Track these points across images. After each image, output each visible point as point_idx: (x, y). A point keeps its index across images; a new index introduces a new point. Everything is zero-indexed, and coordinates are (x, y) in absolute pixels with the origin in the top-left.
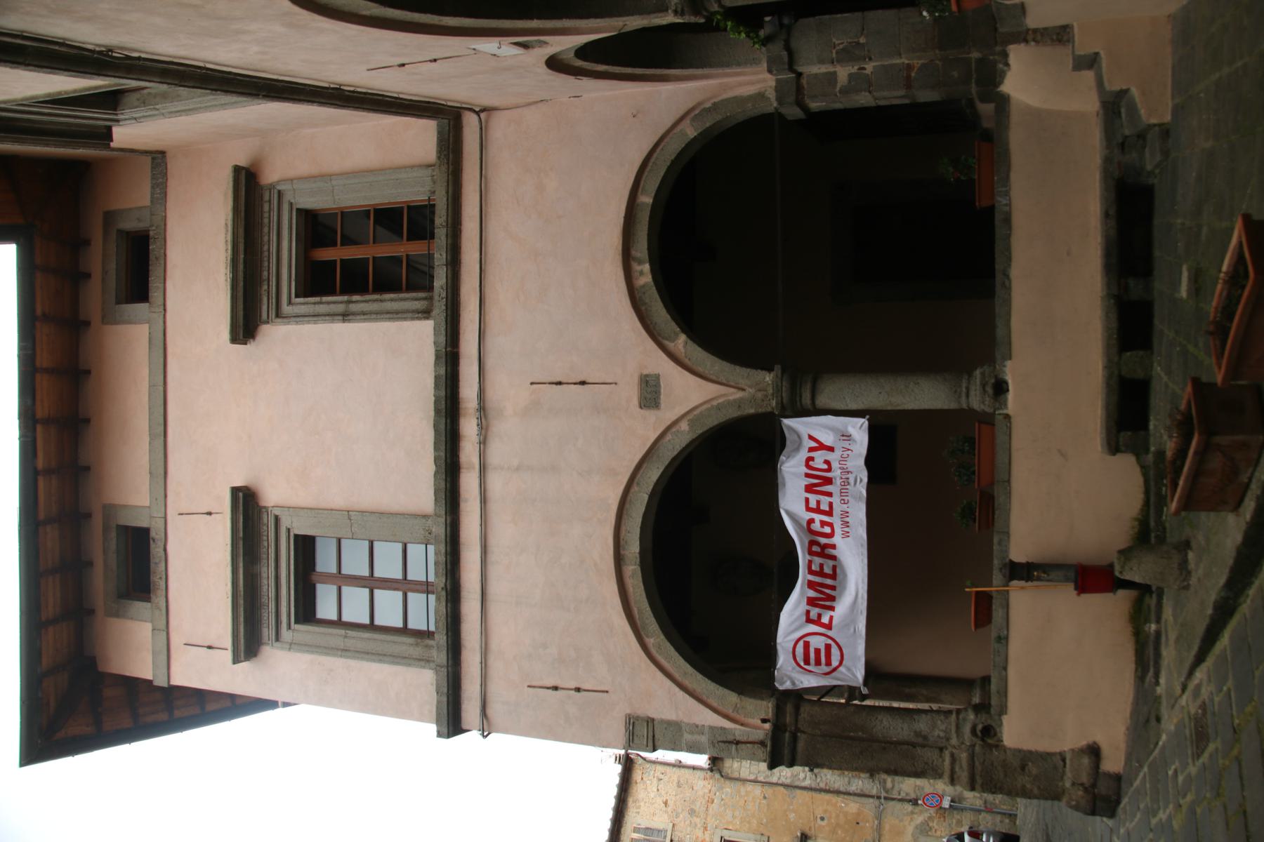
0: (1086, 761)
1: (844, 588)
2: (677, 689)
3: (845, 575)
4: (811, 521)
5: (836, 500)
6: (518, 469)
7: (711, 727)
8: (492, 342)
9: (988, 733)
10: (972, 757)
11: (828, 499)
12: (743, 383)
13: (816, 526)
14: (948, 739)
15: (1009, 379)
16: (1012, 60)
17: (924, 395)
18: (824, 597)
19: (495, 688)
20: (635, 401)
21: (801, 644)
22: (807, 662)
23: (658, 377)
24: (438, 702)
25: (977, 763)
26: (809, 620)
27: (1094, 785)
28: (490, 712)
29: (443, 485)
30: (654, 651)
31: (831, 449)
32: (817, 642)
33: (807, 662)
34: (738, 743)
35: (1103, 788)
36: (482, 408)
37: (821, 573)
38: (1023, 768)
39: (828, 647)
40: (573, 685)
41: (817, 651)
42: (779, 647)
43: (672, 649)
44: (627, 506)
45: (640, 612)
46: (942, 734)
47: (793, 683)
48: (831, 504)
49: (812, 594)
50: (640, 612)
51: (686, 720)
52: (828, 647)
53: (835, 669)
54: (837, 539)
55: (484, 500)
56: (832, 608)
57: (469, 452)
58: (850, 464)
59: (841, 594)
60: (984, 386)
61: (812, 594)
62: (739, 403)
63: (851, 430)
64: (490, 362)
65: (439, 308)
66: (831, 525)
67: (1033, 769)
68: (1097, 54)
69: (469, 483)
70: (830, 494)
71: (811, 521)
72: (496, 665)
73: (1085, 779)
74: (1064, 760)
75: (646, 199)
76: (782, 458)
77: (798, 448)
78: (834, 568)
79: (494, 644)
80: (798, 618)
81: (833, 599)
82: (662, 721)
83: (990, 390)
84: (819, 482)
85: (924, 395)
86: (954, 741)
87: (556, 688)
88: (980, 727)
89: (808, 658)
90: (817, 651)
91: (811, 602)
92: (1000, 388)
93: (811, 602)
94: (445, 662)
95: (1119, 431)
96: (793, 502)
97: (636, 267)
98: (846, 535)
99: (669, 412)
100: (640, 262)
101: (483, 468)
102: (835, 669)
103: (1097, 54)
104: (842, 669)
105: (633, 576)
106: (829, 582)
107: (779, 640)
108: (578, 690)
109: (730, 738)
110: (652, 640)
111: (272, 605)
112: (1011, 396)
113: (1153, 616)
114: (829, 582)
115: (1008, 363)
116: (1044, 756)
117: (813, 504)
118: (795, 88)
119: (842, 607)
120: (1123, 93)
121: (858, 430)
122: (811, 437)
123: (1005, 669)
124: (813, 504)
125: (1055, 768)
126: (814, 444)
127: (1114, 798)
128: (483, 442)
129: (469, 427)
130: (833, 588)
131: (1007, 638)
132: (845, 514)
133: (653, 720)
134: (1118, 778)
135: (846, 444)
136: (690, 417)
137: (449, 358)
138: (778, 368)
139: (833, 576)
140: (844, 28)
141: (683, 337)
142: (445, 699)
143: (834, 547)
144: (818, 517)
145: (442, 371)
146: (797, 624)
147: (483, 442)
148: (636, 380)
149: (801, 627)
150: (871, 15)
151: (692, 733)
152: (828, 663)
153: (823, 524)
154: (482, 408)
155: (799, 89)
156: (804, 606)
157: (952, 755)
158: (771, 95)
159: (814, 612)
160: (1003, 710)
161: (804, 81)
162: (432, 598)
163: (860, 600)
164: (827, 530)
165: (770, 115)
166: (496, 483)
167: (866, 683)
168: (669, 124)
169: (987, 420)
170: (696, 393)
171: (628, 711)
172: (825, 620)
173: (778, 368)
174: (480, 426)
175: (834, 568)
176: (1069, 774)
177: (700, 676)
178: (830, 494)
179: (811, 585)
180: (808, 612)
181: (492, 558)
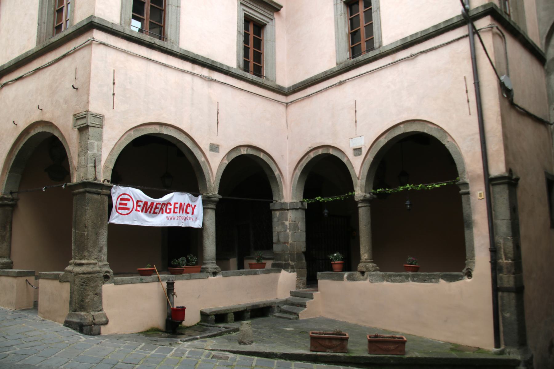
0: (104, 320)
1: (149, 217)
2: (116, 142)
3: (153, 217)
4: (171, 205)
5: (178, 215)
6: (193, 89)
7: (101, 155)
8: (229, 90)
9: (106, 278)
10: (98, 272)
11: (178, 212)
12: (215, 183)
13: (169, 207)
14: (100, 261)
15: (217, 277)
16: (292, 274)
17: (210, 246)
18: (147, 209)
19: (112, 54)
20: (212, 142)
21: (129, 198)
22: (122, 199)
23: (218, 152)
24: (109, 22)
25: (96, 274)
26: (138, 202)
27: (95, 324)
28: (102, 47)
29: (191, 56)
30: (129, 133)
31: (193, 214)
32: (130, 204)
33: (122, 199)
34: (95, 167)
35: (95, 328)
36: (211, 80)
37: (156, 208)
38: (96, 294)
39: (128, 209)
40: (115, 92)
41: (126, 204)
42: (127, 188)
43: (129, 142)
44: (179, 132)
45: (143, 130)
46: (102, 258)
47: (114, 193)
48: (176, 213)
49: (149, 204)
50: (143, 130)
51: (103, 144)
52: (128, 209)
53: (117, 211)
54: (165, 215)
55: (183, 71)
56: (142, 211)
57: (198, 70)
58: (190, 221)
59: (147, 215)
60: (216, 268)
61: (149, 204)
62: (210, 181)
63: (198, 221)
64: (224, 87)
65: (241, 73)
66: (170, 212)
67: (96, 298)
68: (312, 298)
69: (187, 66)
70: (180, 213)
71: (171, 205)
72: (122, 57)
73: (97, 320)
74: (101, 310)
75: (262, 156)
76: (190, 195)
77: (192, 201)
78: (156, 213)
79: (131, 59)
80: (139, 198)
81: (146, 212)
82: (102, 132)
83: (215, 270)
84: (183, 208)
85: (210, 246)
86: (100, 264)
87: (114, 84)
88: (108, 274)
89: (124, 200)
90: (126, 204)
91: (146, 203)
92: (215, 274)
93: (146, 203)
94: (126, 32)
95: (215, 315)
96: (175, 198)
97: (246, 149)
98: (168, 218)
99: (208, 153)
100: (247, 150)
101: (193, 74)
102: (117, 211)
103: (312, 298)
104: (117, 214)
105: (155, 129)
106: (152, 211)
107: (130, 188)
108: (114, 94)
109: (97, 164)
110: (132, 133)
111: (262, 12)
112: (213, 278)
113: (201, 336)
114: (152, 211)
115: (222, 276)
116: (101, 302)
117: (177, 206)
118: (284, 209)
119: (142, 215)
120: (305, 306)
121: (197, 224)
122: (195, 206)
123: (131, 283)
124: (177, 206)
125: (97, 307)
126: (193, 206)
127: (92, 333)
128: (201, 77)
129: (205, 72)
130: (150, 212)
131: (142, 283)
132: (174, 218)
133: (102, 128)
134: (99, 334)
135: (194, 219)
136: (206, 162)
137: (227, 72)
138: (220, 197)
139: (154, 213)
140: (302, 225)
141: (227, 163)
142: (110, 26)
143: (162, 213)
144: (172, 207)
145: (225, 68)
146: (137, 197)
147: (201, 77)
148: (218, 144)
149: (135, 198)
150: (305, 233)
151: (98, 146)
152: (120, 208)
153: (170, 209)
154: (211, 80)
155: (285, 210)
156: (144, 200)
157: (96, 264)
158: (282, 201)
159: (141, 204)
160: (116, 283)
161: (286, 211)
162: (137, 30)
163: (146, 223)
164: (168, 211)
165: (272, 199)
166: (188, 78)
167: (111, 224)
168: (280, 167)
169: (203, 270)
170: (214, 165)
171: (106, 117)
172: (139, 208)
173: (220, 197)
174: (206, 77)
175: (156, 213)
176: (97, 313)
177: (119, 152)
178: (180, 213)
179: (152, 204)
180: (142, 202)
181: (163, 68)
